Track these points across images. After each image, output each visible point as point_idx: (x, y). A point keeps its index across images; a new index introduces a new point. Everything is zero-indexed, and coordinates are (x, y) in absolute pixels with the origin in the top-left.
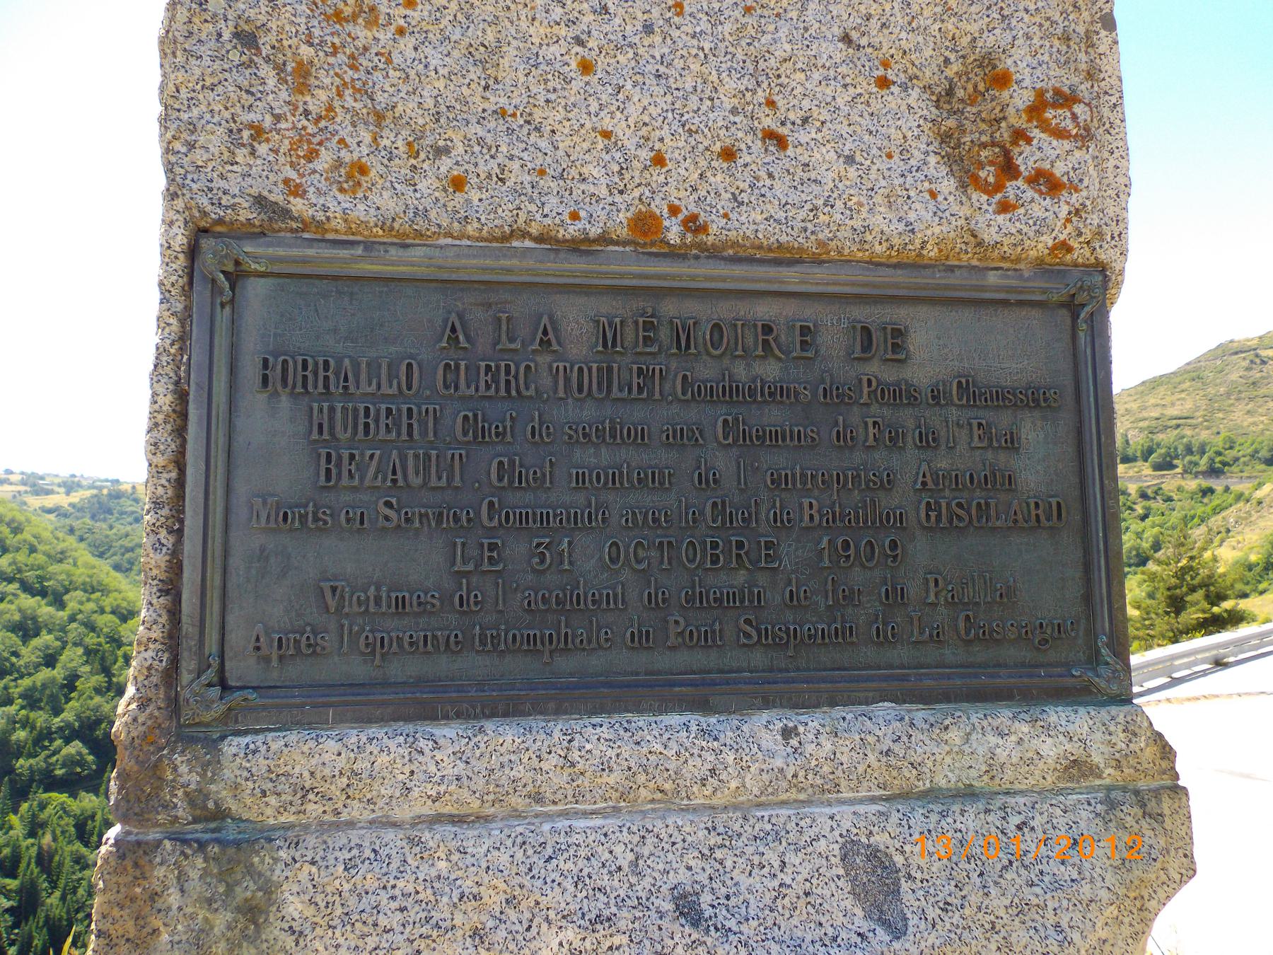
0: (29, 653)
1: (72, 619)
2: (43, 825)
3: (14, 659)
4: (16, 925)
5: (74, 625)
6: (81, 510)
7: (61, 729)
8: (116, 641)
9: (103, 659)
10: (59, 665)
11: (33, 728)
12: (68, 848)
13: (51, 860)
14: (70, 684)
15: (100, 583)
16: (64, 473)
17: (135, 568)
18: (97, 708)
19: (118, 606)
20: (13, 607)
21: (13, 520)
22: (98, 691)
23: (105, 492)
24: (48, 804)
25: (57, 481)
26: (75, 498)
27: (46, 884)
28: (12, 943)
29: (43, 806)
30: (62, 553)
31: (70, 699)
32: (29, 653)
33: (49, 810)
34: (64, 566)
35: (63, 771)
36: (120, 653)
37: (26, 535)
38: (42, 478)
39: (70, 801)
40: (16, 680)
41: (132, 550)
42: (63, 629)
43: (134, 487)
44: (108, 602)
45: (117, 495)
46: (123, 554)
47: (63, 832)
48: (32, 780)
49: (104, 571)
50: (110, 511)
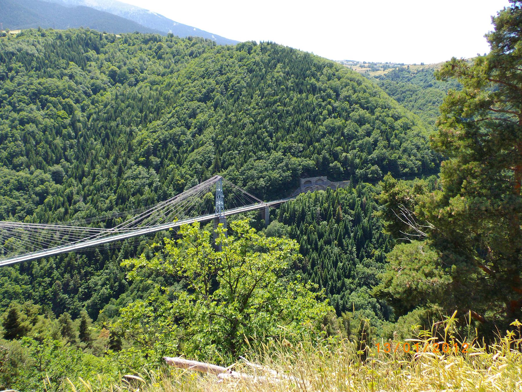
0: (361, 131)
1: (377, 119)
2: (363, 194)
3: (356, 133)
4: (353, 226)
5: (377, 121)
6: (388, 77)
7: (371, 160)
8: (392, 128)
9: (387, 135)
10: (372, 136)
11: (361, 159)
12: (371, 203)
13: (365, 206)
14: (375, 143)
15: (388, 105)
16: (384, 62)
17: (406, 100)
18: (384, 153)
19: (394, 114)
20: (357, 114)
21: (358, 80)
22: (385, 147)
23: (397, 69)
24: (365, 187)
25: (381, 65)
26: (386, 72)
27: (363, 215)
28: (352, 232)
29: (363, 187)
30: (375, 93)
31: (375, 149)
32: (361, 131)
33: (365, 189)
34: (375, 98)
35: (371, 175)
36: (394, 133)
37: (363, 86)
38: (376, 65)
39: (372, 187)
40: (357, 141)
41: (405, 92)
42: (374, 123)
43: (408, 66)
44: (390, 113)
45: (402, 70)
46: (401, 94)
47: (370, 197)
48: (360, 177)
49: (392, 102)
50: (398, 77)
